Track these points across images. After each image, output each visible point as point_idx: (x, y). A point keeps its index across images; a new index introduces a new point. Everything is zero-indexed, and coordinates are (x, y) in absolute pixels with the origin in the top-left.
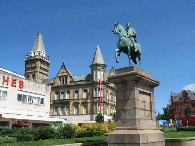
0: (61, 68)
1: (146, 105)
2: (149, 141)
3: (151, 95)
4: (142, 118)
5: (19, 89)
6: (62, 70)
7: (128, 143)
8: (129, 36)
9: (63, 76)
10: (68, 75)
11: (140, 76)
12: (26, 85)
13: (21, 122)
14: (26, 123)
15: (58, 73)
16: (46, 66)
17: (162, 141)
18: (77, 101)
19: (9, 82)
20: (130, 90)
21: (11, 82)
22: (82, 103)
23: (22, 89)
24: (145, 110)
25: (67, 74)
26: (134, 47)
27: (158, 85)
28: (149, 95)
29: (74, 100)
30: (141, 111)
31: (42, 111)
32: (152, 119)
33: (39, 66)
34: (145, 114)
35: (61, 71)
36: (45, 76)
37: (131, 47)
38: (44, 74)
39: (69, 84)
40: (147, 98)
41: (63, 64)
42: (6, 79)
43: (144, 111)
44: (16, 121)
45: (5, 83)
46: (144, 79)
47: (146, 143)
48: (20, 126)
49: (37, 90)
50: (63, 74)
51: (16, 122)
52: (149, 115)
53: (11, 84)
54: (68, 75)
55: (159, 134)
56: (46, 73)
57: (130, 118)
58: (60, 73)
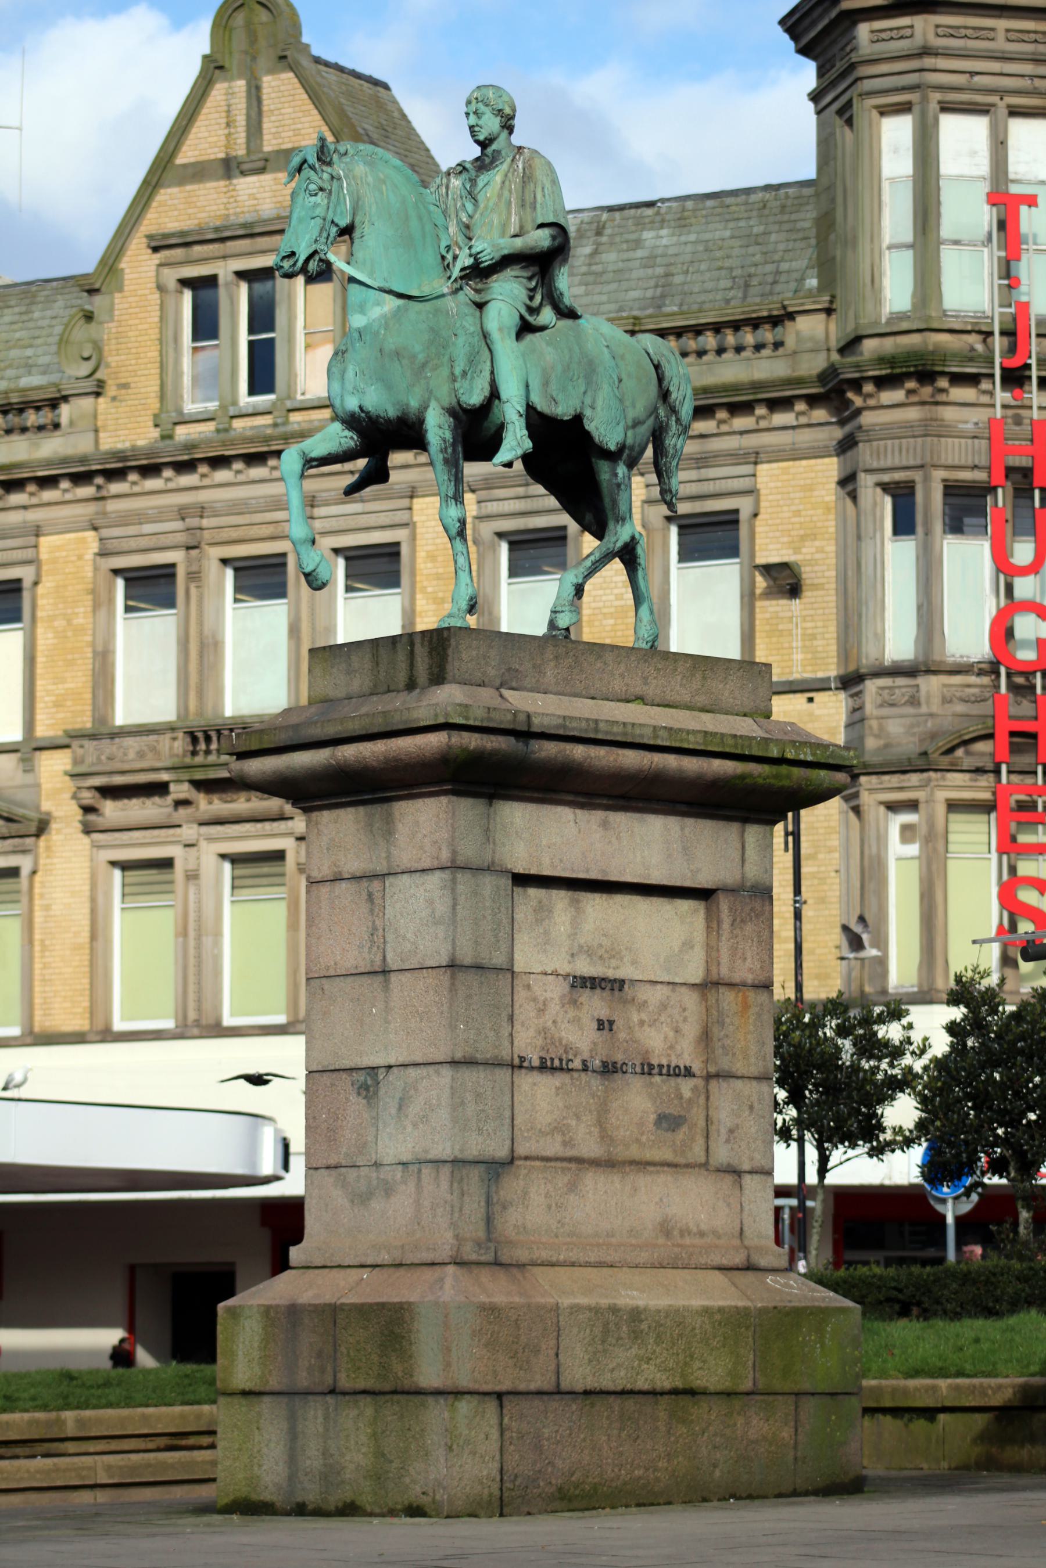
0: (213, 69)
6: (229, 93)
15: (163, 171)
43: (595, 1082)
50: (259, 195)
58: (198, 172)
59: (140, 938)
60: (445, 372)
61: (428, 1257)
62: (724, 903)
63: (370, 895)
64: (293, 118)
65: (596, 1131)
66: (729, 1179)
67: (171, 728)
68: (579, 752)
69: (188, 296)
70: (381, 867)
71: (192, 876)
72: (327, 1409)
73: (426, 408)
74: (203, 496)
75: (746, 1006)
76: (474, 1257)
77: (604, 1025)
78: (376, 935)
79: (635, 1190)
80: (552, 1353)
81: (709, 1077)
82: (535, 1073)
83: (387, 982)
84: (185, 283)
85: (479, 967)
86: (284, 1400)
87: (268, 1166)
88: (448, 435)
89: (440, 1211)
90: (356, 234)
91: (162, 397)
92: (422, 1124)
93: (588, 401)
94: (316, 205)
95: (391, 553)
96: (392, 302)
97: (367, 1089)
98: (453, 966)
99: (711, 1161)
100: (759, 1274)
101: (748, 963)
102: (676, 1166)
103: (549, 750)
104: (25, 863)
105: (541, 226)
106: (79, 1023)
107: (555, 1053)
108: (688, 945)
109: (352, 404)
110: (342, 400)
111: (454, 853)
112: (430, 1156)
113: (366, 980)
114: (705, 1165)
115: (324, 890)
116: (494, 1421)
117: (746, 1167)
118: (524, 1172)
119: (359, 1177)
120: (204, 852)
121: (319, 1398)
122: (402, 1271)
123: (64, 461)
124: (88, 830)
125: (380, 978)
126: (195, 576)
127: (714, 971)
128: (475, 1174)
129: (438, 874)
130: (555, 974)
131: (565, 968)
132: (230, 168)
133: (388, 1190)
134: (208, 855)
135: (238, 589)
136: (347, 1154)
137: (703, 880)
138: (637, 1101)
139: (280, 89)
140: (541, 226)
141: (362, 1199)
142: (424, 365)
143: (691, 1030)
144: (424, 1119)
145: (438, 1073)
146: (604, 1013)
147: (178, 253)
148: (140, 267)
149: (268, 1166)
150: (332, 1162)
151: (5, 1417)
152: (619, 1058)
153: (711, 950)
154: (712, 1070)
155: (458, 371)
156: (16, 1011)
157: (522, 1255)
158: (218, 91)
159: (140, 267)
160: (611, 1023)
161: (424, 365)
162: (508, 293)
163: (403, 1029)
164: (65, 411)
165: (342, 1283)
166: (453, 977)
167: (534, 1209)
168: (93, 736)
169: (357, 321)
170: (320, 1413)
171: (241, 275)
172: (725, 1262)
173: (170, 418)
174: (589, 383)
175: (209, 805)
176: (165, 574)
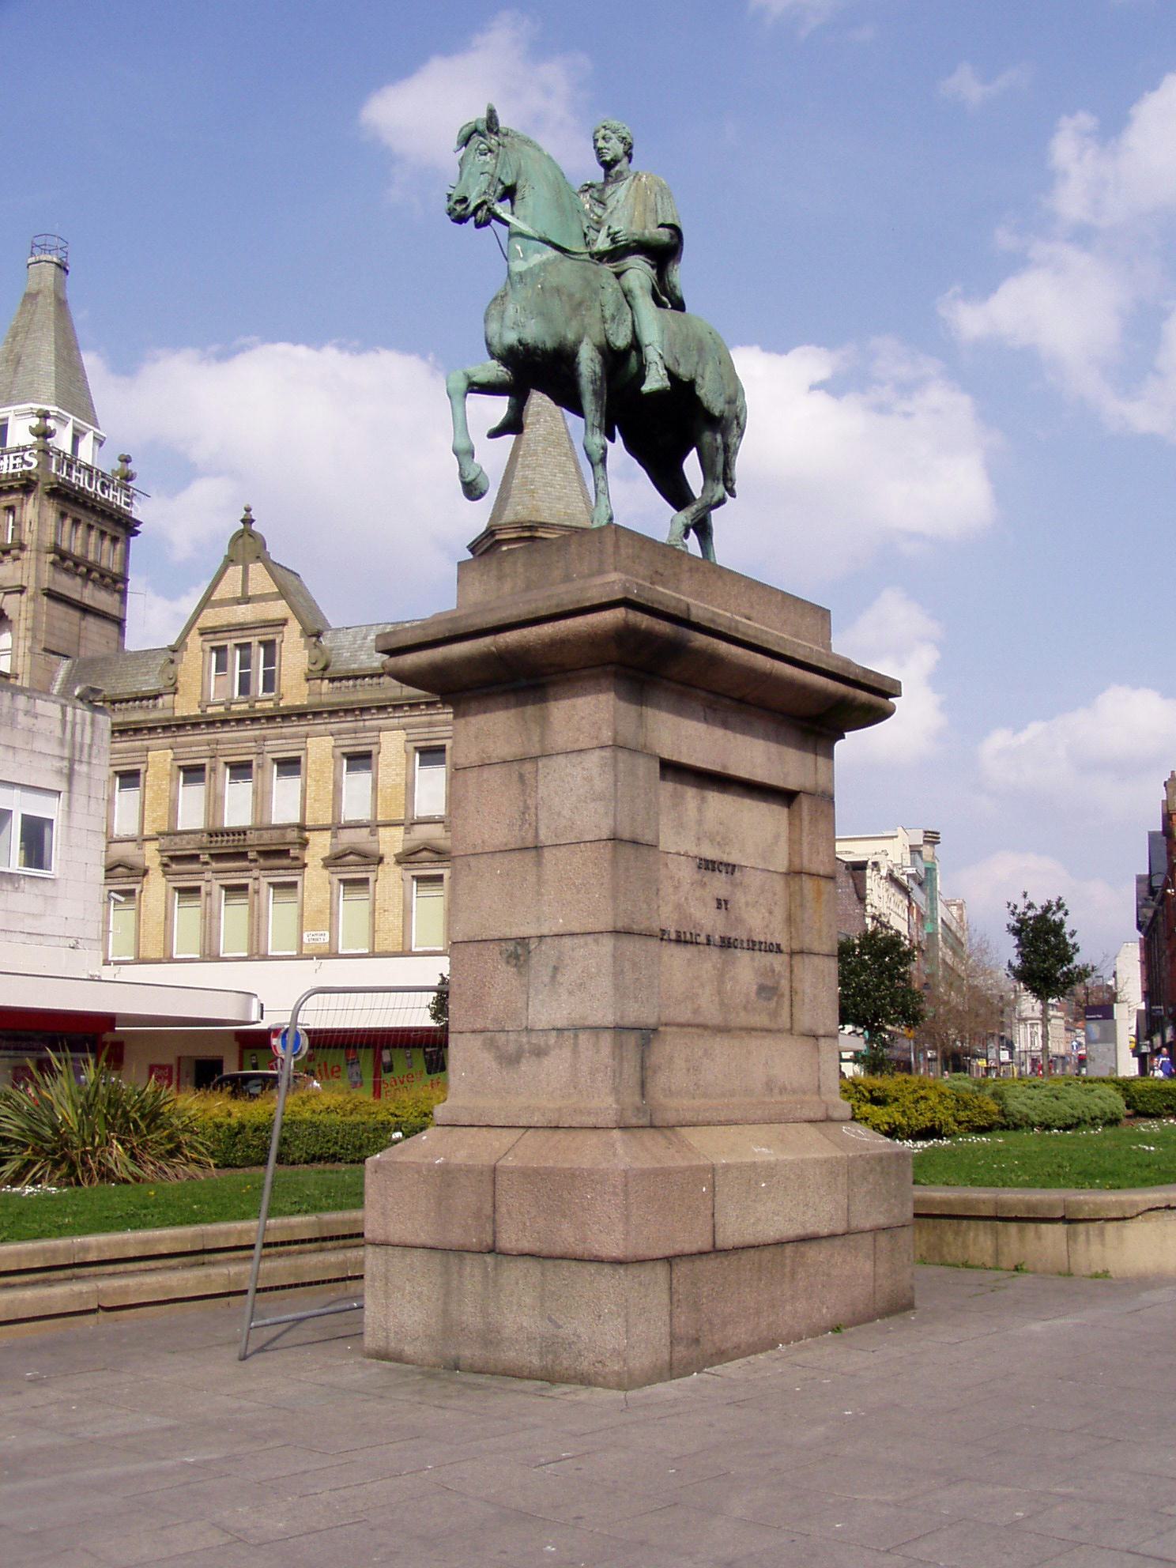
0: (230, 561)
1: (740, 899)
2: (729, 1235)
6: (235, 572)
7: (526, 1245)
9: (242, 627)
10: (284, 622)
11: (663, 627)
15: (206, 602)
16: (107, 543)
17: (882, 1220)
20: (573, 757)
22: (406, 858)
25: (278, 609)
26: (636, 345)
27: (877, 715)
29: (336, 827)
31: (29, 925)
35: (231, 585)
36: (91, 622)
38: (86, 610)
39: (294, 691)
40: (755, 830)
41: (247, 521)
43: (714, 954)
46: (714, 661)
47: (688, 1248)
50: (244, 613)
54: (284, 622)
55: (851, 1170)
57: (560, 1018)
58: (222, 603)
59: (187, 918)
60: (598, 315)
61: (590, 1121)
62: (805, 803)
63: (521, 777)
64: (260, 580)
65: (716, 999)
66: (812, 1041)
67: (201, 831)
68: (723, 647)
69: (214, 655)
70: (535, 750)
71: (209, 894)
72: (486, 1268)
73: (580, 342)
74: (218, 736)
75: (819, 893)
76: (634, 1121)
77: (721, 904)
78: (527, 814)
79: (749, 1052)
80: (709, 1213)
81: (792, 954)
82: (673, 945)
83: (540, 856)
84: (213, 648)
85: (635, 842)
86: (438, 1255)
87: (254, 1017)
88: (598, 369)
89: (600, 1076)
90: (518, 196)
91: (202, 694)
93: (700, 371)
94: (486, 163)
95: (296, 761)
96: (551, 253)
97: (517, 957)
98: (615, 839)
99: (796, 1027)
100: (836, 1124)
101: (820, 857)
102: (769, 1031)
103: (700, 640)
104: (138, 887)
105: (662, 226)
106: (159, 955)
108: (777, 837)
109: (511, 338)
110: (500, 337)
111: (616, 732)
112: (590, 1022)
113: (517, 855)
114: (791, 1031)
115: (472, 775)
117: (821, 1032)
118: (669, 1038)
119: (508, 1041)
120: (212, 883)
121: (476, 1256)
122: (560, 1134)
123: (159, 720)
124: (165, 874)
125: (533, 853)
126: (213, 770)
127: (797, 861)
128: (632, 1039)
129: (597, 753)
130: (686, 855)
131: (694, 851)
132: (238, 601)
133: (540, 1052)
134: (216, 886)
135: (231, 777)
136: (494, 1020)
137: (791, 784)
139: (257, 569)
140: (662, 226)
141: (510, 1060)
142: (580, 304)
143: (780, 913)
145: (596, 941)
146: (722, 894)
147: (211, 636)
148: (195, 641)
149: (254, 1017)
150: (478, 1026)
152: (733, 935)
153: (794, 843)
154: (796, 947)
155: (608, 314)
156: (132, 950)
157: (671, 1117)
158: (231, 570)
159: (195, 641)
160: (726, 902)
161: (580, 304)
162: (639, 272)
163: (567, 899)
164: (160, 701)
165: (496, 1144)
166: (615, 848)
168: (168, 834)
169: (518, 266)
170: (477, 1272)
171: (236, 645)
172: (812, 1116)
173: (204, 704)
174: (700, 356)
175: (215, 865)
176: (201, 768)
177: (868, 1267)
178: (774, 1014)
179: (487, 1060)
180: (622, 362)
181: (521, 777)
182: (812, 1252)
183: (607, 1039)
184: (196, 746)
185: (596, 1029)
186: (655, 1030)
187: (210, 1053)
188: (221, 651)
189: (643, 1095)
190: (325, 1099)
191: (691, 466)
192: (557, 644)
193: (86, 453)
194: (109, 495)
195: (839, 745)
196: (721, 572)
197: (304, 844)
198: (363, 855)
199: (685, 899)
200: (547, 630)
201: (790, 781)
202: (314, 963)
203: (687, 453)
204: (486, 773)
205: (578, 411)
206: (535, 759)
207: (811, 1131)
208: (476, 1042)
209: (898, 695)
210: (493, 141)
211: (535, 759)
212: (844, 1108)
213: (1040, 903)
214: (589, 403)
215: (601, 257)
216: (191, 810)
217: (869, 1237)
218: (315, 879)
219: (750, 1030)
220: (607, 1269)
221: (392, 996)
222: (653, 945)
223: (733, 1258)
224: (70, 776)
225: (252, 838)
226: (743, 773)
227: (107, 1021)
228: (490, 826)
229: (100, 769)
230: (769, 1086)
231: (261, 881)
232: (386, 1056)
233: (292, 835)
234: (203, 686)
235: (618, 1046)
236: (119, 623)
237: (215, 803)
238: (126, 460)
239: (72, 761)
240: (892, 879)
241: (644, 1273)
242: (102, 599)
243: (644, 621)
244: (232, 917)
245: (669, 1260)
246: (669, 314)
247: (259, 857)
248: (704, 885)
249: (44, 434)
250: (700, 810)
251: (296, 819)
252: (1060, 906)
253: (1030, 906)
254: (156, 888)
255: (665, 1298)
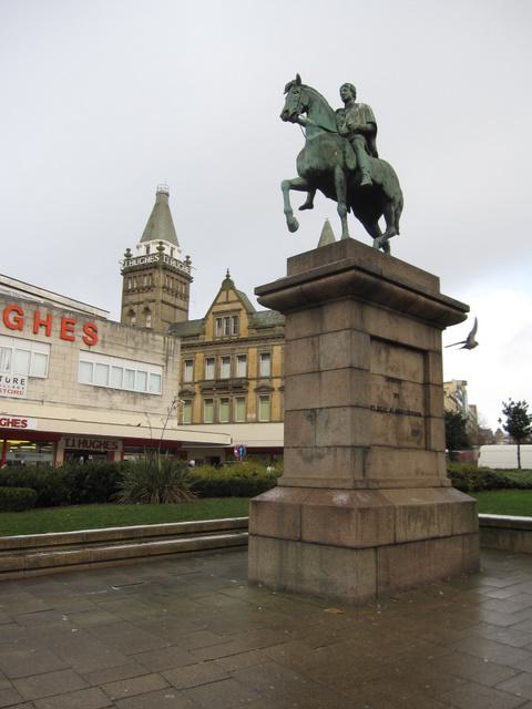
0: (222, 290)
2: (402, 536)
3: (430, 354)
4: (381, 441)
5: (85, 347)
6: (224, 293)
7: (314, 539)
8: (344, 129)
12: (104, 337)
13: (92, 444)
14: (85, 443)
15: (214, 304)
17: (465, 530)
18: (265, 382)
19: (53, 328)
20: (335, 334)
21: (59, 328)
23: (92, 349)
24: (399, 412)
25: (238, 305)
26: (358, 169)
28: (424, 353)
30: (380, 416)
31: (154, 411)
32: (427, 448)
33: (161, 284)
34: (397, 425)
37: (345, 169)
39: (244, 333)
41: (228, 276)
42: (43, 318)
43: (394, 417)
44: (77, 439)
45: (42, 330)
48: (86, 454)
49: (140, 352)
51: (76, 444)
52: (415, 433)
53: (58, 334)
54: (240, 310)
56: (182, 302)
58: (219, 304)
59: (208, 410)
64: (232, 297)
77: (396, 396)
83: (320, 377)
92: (337, 430)
96: (323, 132)
107: (381, 405)
116: (373, 559)
120: (217, 398)
125: (316, 375)
128: (359, 451)
131: (385, 373)
132: (224, 303)
133: (320, 457)
137: (425, 347)
138: (407, 424)
141: (309, 460)
144: (337, 429)
146: (397, 392)
148: (211, 316)
151: (529, 519)
159: (211, 316)
162: (360, 141)
163: (329, 394)
167: (381, 465)
173: (214, 337)
177: (460, 549)
178: (419, 442)
179: (299, 459)
180: (353, 174)
181: (313, 344)
182: (437, 545)
183: (349, 451)
184: (211, 352)
185: (345, 447)
186: (369, 448)
187: (216, 455)
188: (219, 320)
189: (364, 475)
190: (245, 468)
191: (382, 223)
192: (325, 287)
193: (176, 256)
194: (182, 269)
195: (444, 332)
196: (395, 260)
197: (248, 384)
198: (268, 388)
199: (379, 392)
200: (323, 281)
201: (425, 346)
202: (250, 425)
203: (378, 218)
204: (299, 341)
205: (335, 198)
206: (318, 335)
207: (434, 491)
208: (295, 452)
209: (468, 311)
210: (299, 89)
211: (318, 335)
212: (448, 482)
213: (516, 402)
214: (339, 192)
215: (345, 136)
216: (210, 374)
217: (460, 538)
218: (252, 397)
219: (409, 448)
220: (349, 551)
221: (271, 435)
222: (368, 411)
223: (403, 547)
224: (167, 361)
225: (230, 383)
226: (405, 342)
227: (180, 443)
228: (302, 363)
229: (177, 359)
230: (417, 472)
231: (233, 397)
232: (275, 456)
233: (244, 381)
234: (215, 332)
235: (353, 454)
236: (187, 311)
237: (217, 371)
238: (188, 257)
239: (167, 356)
240: (450, 396)
241: (365, 554)
242: (180, 303)
243: (364, 276)
244: (223, 410)
245: (376, 548)
246: (371, 158)
247: (231, 390)
248: (388, 387)
249: (161, 249)
250: (387, 356)
251: (244, 375)
252: (524, 403)
253: (513, 403)
254: (198, 400)
255: (374, 565)
